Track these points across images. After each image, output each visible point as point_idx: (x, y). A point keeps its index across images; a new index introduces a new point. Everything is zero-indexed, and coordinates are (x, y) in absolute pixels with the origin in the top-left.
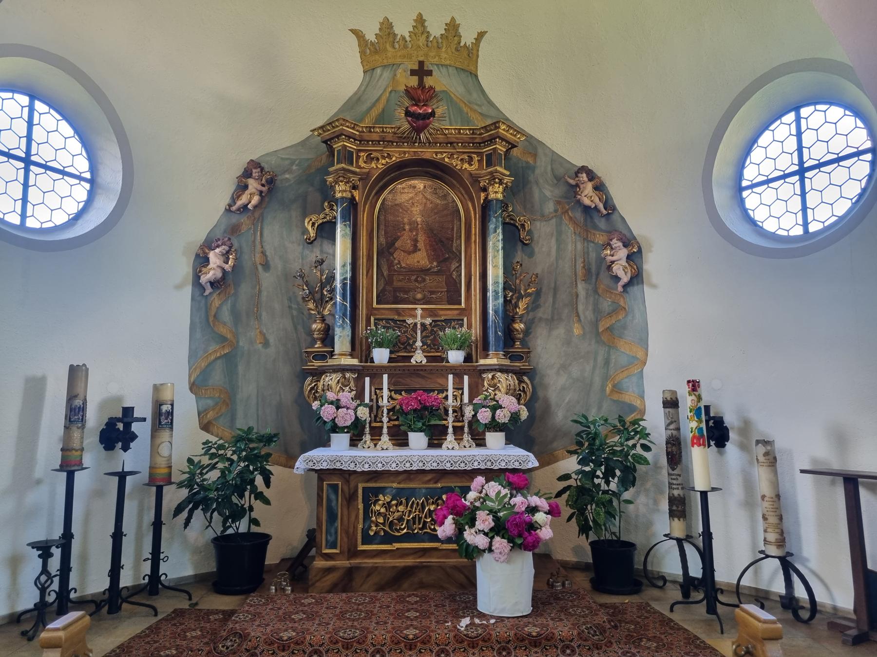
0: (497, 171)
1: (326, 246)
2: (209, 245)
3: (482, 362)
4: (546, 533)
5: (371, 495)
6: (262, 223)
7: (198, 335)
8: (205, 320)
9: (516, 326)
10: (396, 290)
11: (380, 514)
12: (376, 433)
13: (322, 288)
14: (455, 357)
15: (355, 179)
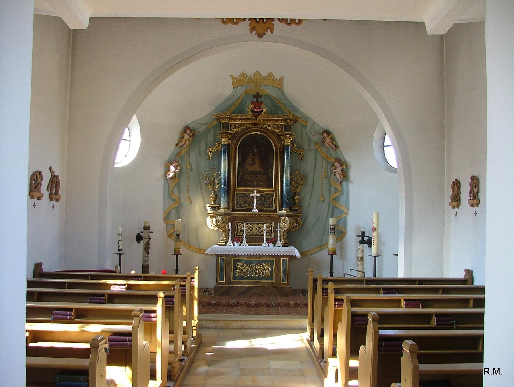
5: (236, 262)
6: (189, 156)
11: (239, 269)
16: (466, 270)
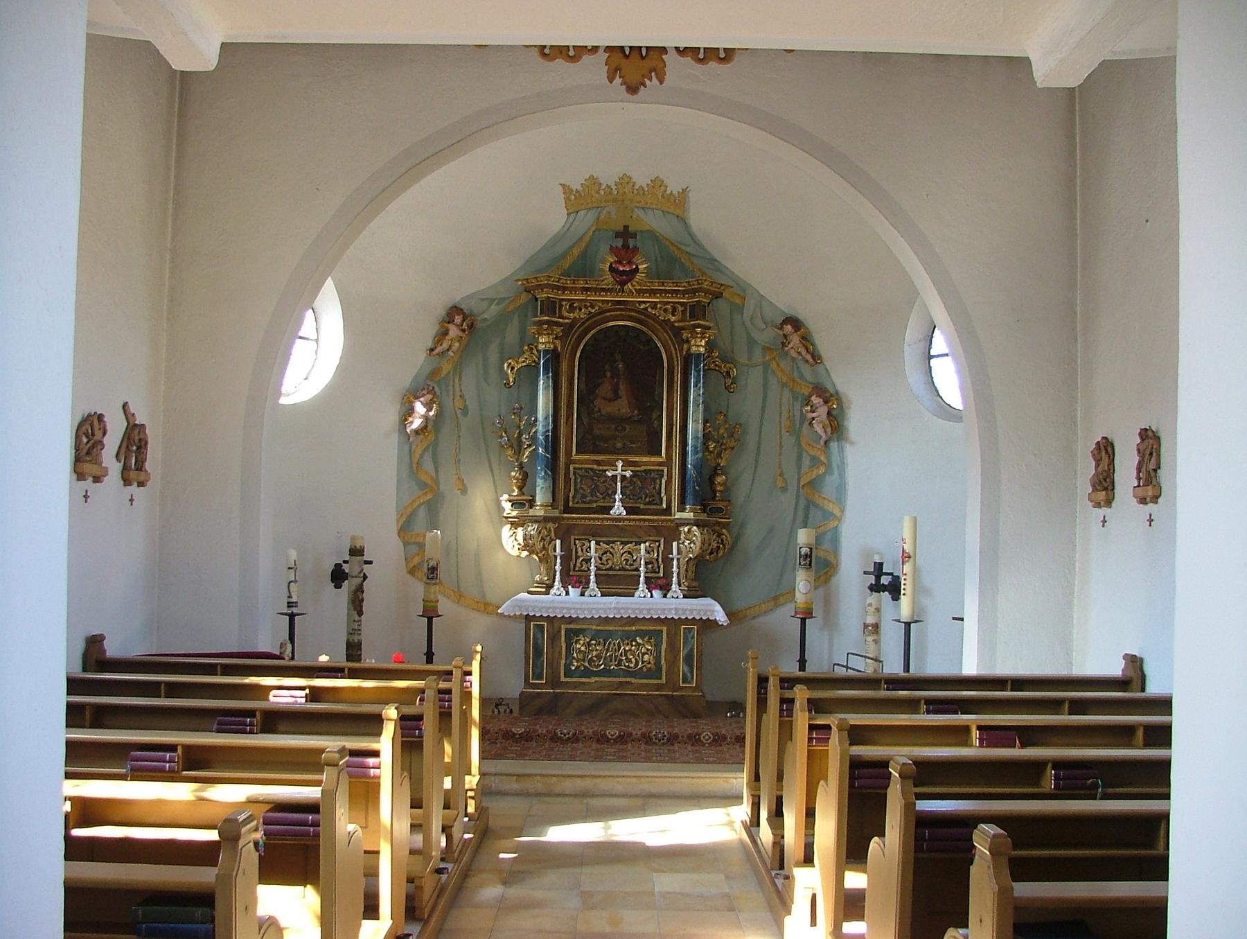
3: (678, 515)
5: (573, 635)
11: (580, 651)
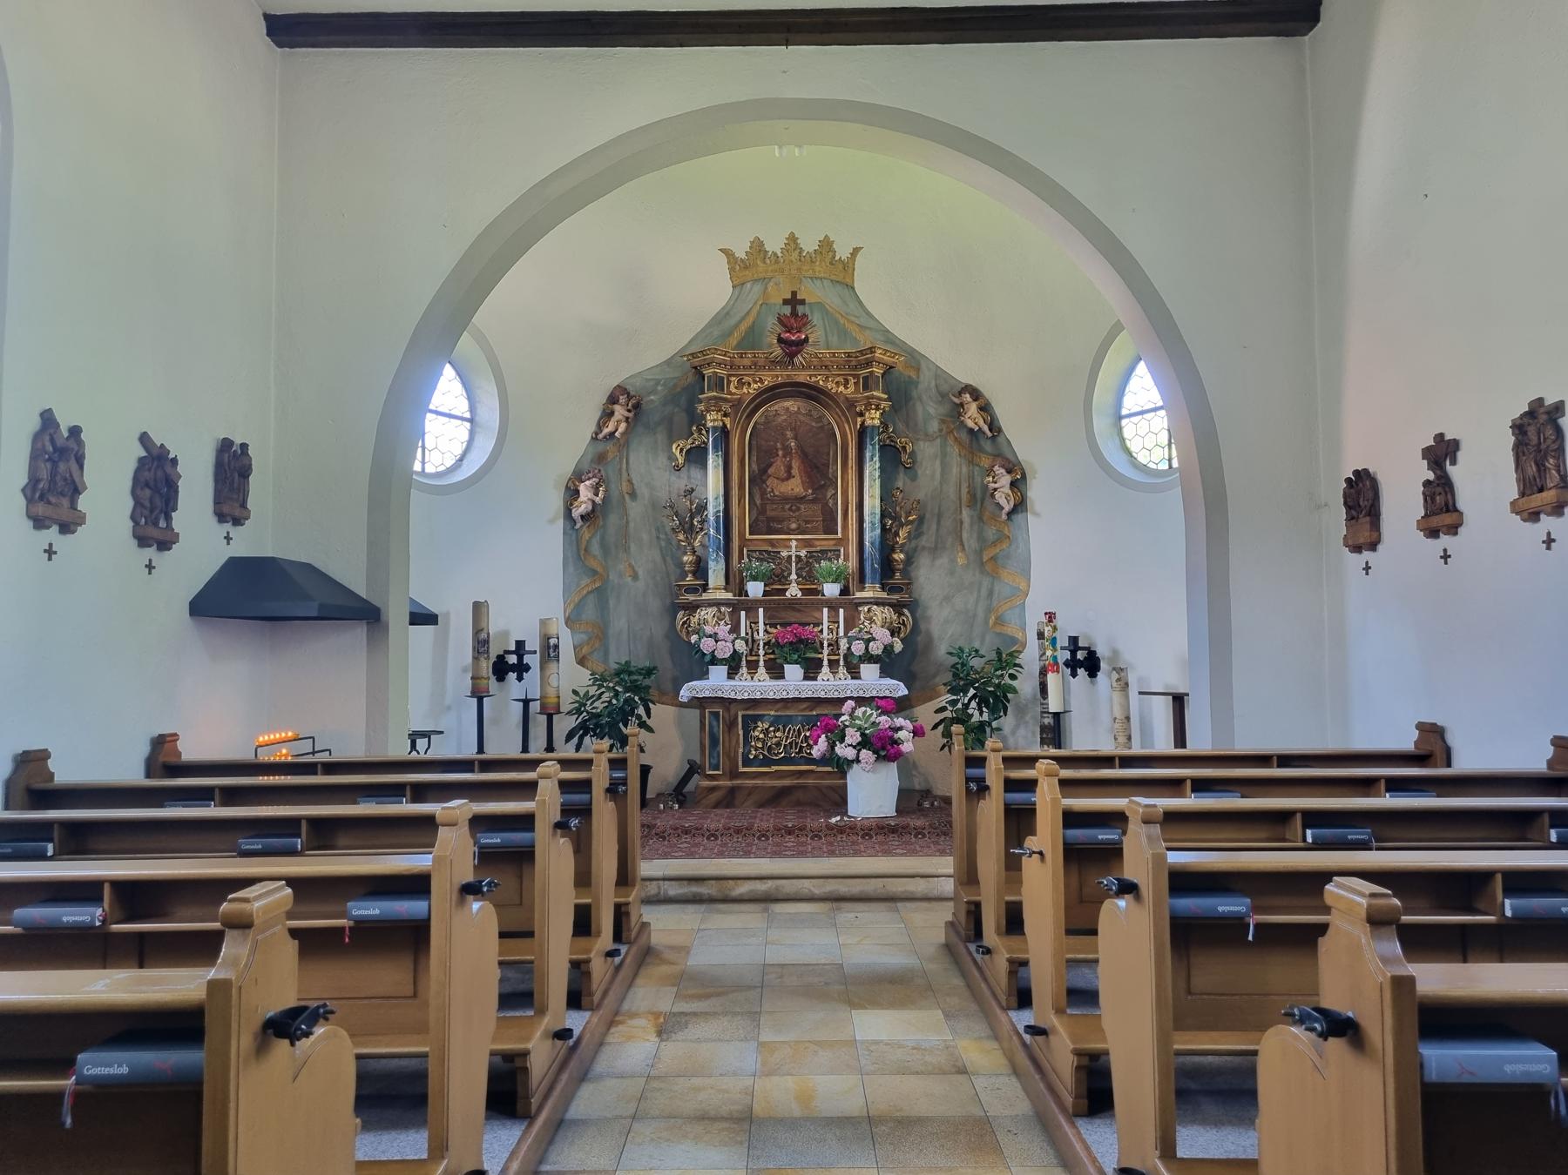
0: (873, 397)
1: (695, 473)
2: (578, 476)
3: (858, 595)
4: (907, 747)
5: (751, 722)
7: (571, 569)
8: (577, 553)
9: (896, 556)
10: (770, 519)
12: (753, 666)
13: (692, 518)
14: (831, 590)
15: (726, 407)
16: (1421, 727)
